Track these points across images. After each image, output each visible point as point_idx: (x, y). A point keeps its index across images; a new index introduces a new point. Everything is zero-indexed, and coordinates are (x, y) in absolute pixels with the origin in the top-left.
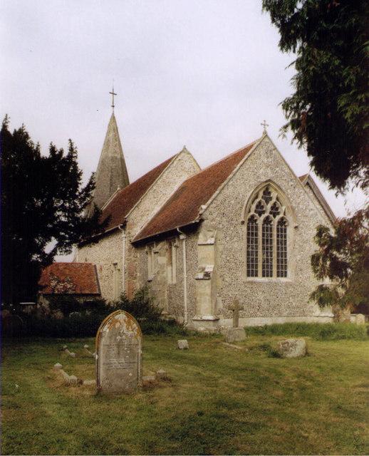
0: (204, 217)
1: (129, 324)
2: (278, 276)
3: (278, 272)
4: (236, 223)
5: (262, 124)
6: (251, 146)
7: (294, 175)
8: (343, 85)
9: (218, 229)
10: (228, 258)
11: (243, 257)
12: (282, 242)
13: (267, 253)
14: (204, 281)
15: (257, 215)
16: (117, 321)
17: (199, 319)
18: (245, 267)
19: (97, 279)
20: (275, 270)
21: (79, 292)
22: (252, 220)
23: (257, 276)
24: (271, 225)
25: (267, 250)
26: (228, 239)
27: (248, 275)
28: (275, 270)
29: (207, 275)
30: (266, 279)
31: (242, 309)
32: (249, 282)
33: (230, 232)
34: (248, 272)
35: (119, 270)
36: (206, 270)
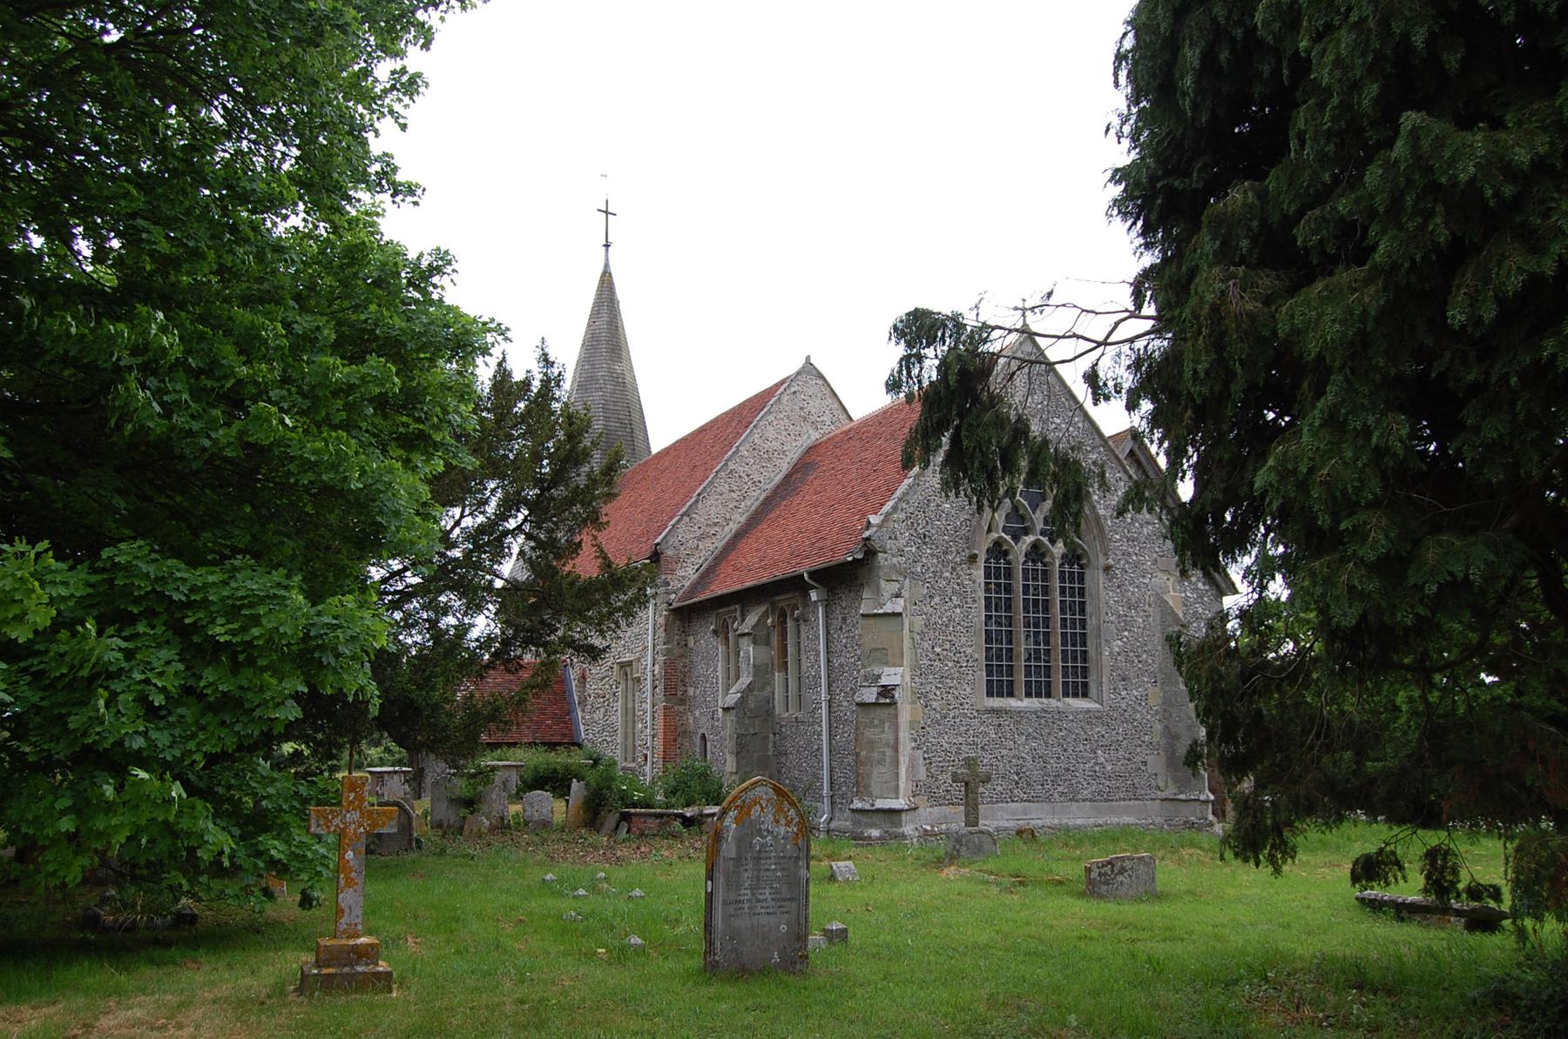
2: (1066, 694)
3: (1065, 684)
5: (1016, 309)
7: (1100, 434)
10: (938, 650)
11: (975, 648)
12: (1077, 606)
13: (1036, 634)
14: (879, 711)
15: (1008, 538)
17: (868, 807)
20: (1058, 679)
22: (998, 550)
23: (1011, 694)
24: (1009, 563)
25: (1040, 629)
26: (937, 599)
28: (1058, 679)
30: (1033, 703)
32: (993, 711)
34: (987, 693)
35: (638, 680)
36: (883, 682)
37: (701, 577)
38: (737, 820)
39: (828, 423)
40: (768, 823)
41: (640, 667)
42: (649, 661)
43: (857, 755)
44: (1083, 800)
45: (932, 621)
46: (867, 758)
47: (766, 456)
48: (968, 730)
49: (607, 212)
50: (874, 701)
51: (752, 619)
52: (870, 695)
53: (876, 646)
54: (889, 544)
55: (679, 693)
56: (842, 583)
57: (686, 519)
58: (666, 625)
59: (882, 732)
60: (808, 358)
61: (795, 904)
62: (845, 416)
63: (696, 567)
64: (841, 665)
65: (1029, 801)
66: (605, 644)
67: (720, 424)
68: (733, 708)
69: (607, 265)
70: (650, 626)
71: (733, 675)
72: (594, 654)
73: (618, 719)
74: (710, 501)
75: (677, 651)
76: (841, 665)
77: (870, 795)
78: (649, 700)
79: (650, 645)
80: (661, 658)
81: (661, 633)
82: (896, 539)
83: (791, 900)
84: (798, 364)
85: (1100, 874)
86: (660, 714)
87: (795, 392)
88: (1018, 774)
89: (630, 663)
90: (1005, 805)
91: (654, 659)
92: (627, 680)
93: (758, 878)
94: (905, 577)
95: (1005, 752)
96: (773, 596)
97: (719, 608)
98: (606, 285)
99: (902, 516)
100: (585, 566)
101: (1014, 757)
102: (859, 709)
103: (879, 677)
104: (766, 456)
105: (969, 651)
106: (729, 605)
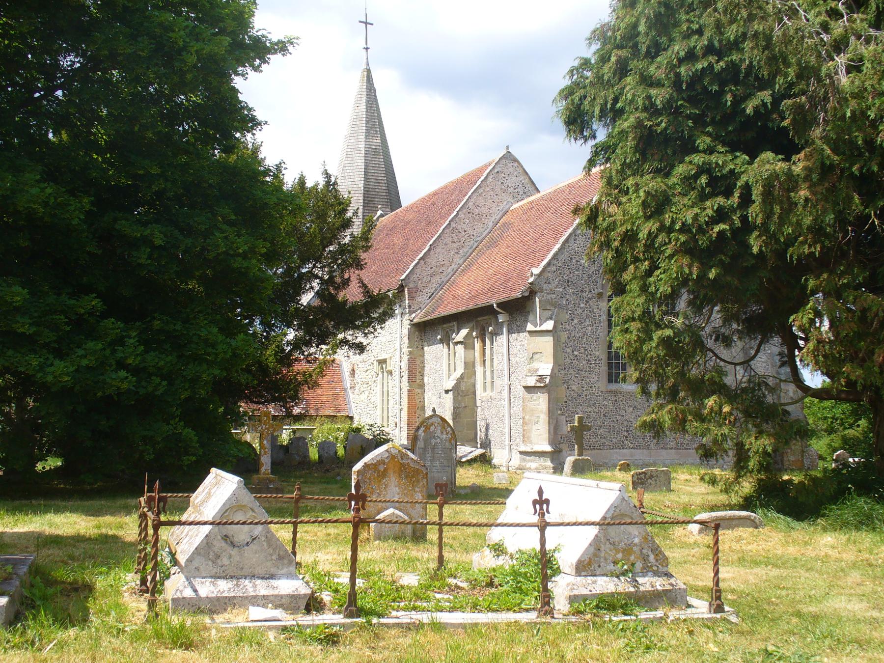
4: (590, 296)
6: (486, 166)
8: (97, 13)
9: (560, 306)
10: (576, 353)
18: (604, 369)
26: (576, 321)
27: (610, 381)
32: (611, 392)
33: (579, 311)
34: (610, 375)
36: (540, 373)
38: (424, 431)
40: (438, 433)
41: (392, 363)
42: (398, 359)
43: (524, 418)
44: (670, 449)
45: (573, 335)
46: (530, 420)
47: (477, 217)
48: (595, 403)
49: (366, 23)
50: (533, 385)
51: (464, 332)
53: (536, 351)
54: (545, 286)
55: (418, 381)
56: (517, 310)
57: (422, 262)
58: (409, 335)
59: (538, 404)
61: (450, 468)
62: (533, 188)
63: (429, 295)
64: (517, 363)
65: (635, 448)
66: (368, 341)
67: (447, 191)
68: (451, 390)
71: (451, 368)
72: (361, 348)
73: (377, 399)
76: (517, 363)
77: (531, 443)
78: (398, 386)
81: (406, 340)
82: (549, 283)
83: (448, 466)
85: (638, 479)
87: (498, 172)
88: (627, 431)
90: (618, 450)
92: (383, 372)
93: (433, 457)
94: (555, 307)
95: (619, 418)
96: (477, 317)
97: (444, 324)
99: (554, 268)
100: (352, 294)
101: (626, 420)
103: (537, 370)
104: (477, 217)
106: (450, 322)
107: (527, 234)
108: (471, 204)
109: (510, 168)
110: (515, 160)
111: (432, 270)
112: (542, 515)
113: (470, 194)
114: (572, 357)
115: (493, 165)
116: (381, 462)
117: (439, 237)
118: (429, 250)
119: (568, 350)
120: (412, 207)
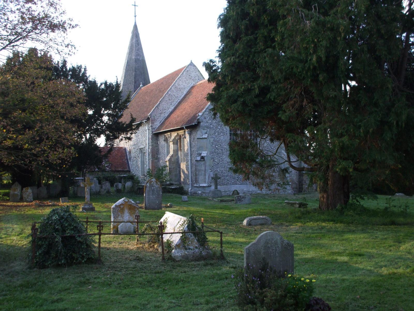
0: (201, 120)
1: (157, 183)
9: (210, 128)
10: (217, 147)
14: (201, 162)
16: (152, 181)
17: (198, 186)
19: (127, 160)
21: (113, 169)
26: (216, 134)
29: (203, 158)
31: (220, 178)
35: (145, 153)
36: (202, 155)
37: (161, 125)
39: (197, 79)
43: (196, 173)
52: (199, 158)
54: (204, 120)
57: (157, 108)
60: (191, 61)
69: (135, 23)
70: (147, 138)
74: (163, 103)
75: (155, 145)
76: (193, 151)
77: (199, 183)
79: (147, 143)
80: (150, 147)
81: (150, 140)
84: (188, 63)
86: (151, 162)
89: (142, 148)
91: (149, 147)
98: (135, 27)
102: (196, 162)
105: (225, 147)
107: (198, 98)
108: (176, 84)
109: (192, 67)
110: (194, 66)
111: (161, 112)
112: (100, 230)
113: (176, 80)
114: (215, 148)
115: (185, 68)
116: (122, 204)
117: (164, 98)
118: (160, 103)
119: (214, 146)
120: (154, 83)
